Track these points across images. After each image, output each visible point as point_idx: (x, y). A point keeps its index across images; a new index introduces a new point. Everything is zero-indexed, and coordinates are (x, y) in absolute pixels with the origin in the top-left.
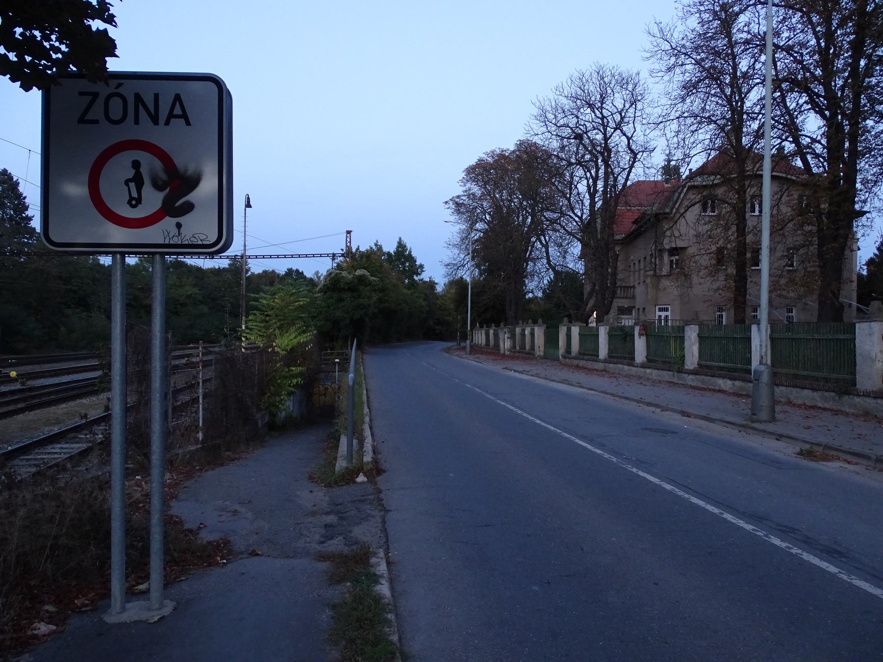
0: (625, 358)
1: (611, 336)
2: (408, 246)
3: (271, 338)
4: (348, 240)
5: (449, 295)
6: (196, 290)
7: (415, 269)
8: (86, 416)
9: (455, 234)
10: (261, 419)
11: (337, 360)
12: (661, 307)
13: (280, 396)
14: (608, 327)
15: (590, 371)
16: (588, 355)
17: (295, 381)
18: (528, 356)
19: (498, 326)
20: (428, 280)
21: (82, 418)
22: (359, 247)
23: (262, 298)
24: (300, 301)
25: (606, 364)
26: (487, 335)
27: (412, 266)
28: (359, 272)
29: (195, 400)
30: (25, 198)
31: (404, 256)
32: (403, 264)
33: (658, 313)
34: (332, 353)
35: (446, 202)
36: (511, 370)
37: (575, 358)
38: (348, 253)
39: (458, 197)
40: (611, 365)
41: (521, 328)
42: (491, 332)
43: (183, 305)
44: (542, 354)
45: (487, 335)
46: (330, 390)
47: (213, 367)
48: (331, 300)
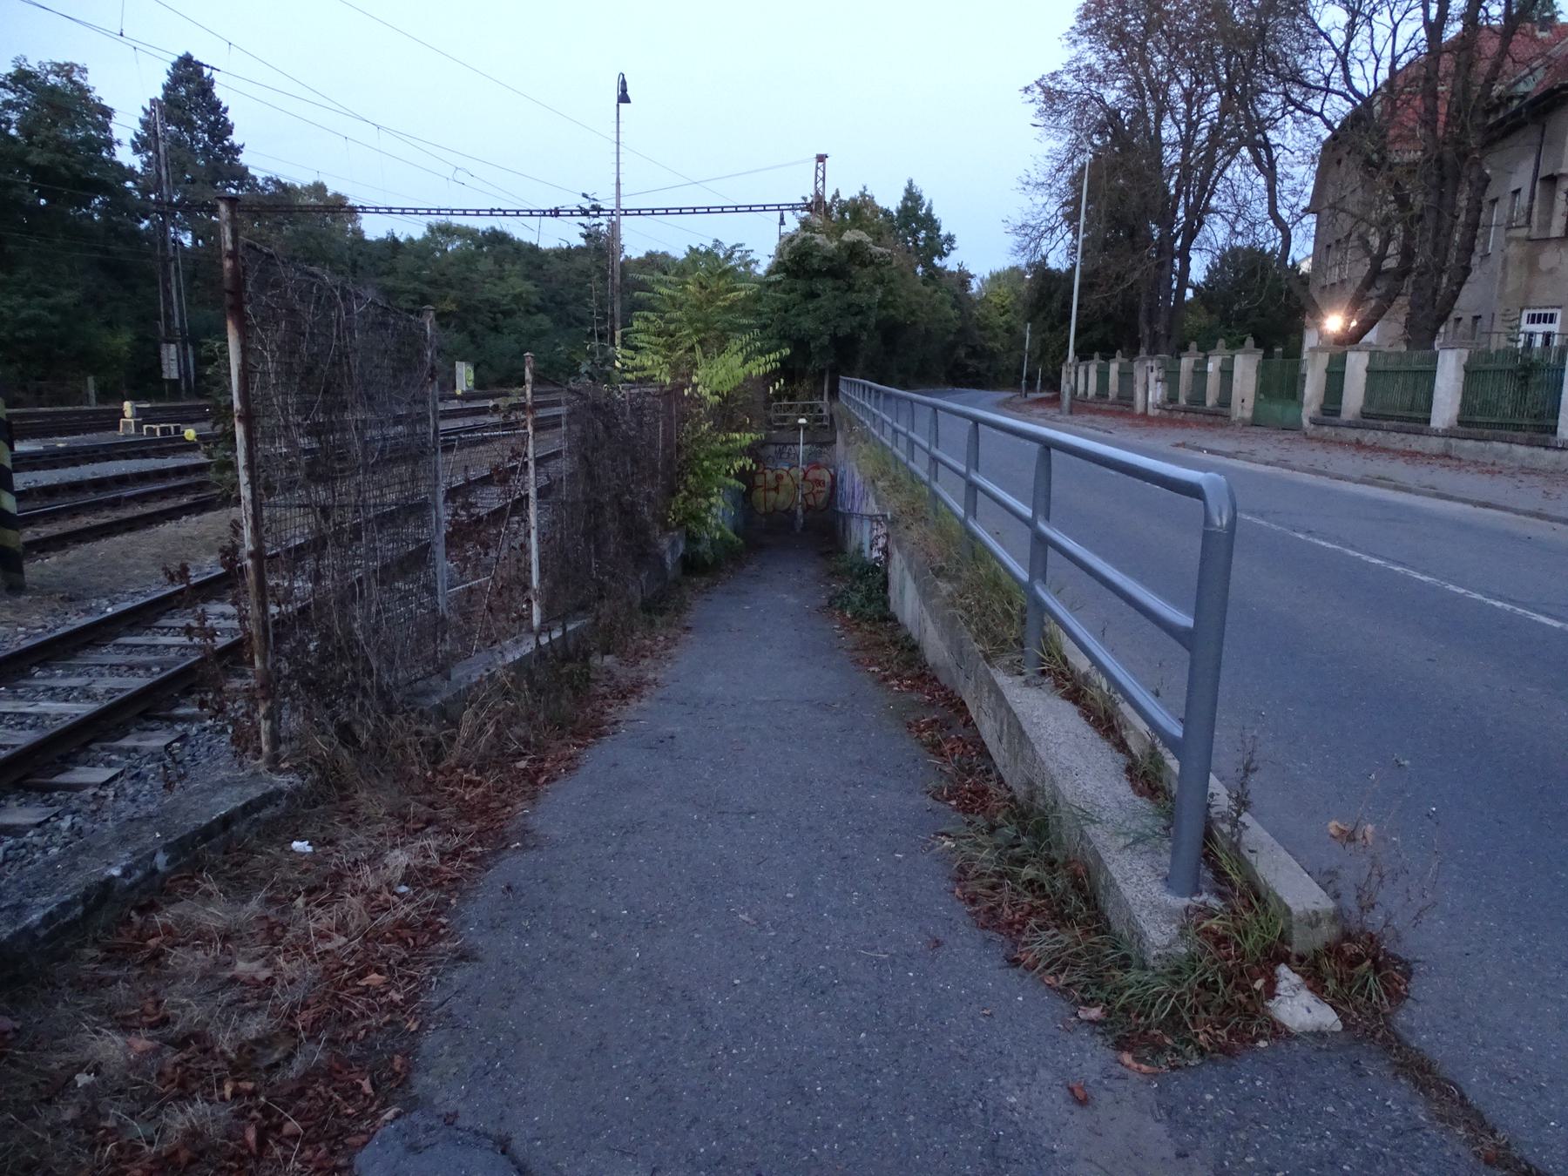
0: (1518, 428)
1: (1472, 373)
2: (926, 198)
3: (683, 371)
4: (820, 174)
5: (996, 300)
6: (528, 286)
7: (937, 244)
8: (184, 571)
9: (1043, 160)
10: (670, 548)
11: (802, 421)
12: (1537, 312)
13: (707, 496)
14: (1465, 353)
15: (1413, 455)
16: (1391, 418)
17: (738, 464)
18: (1210, 419)
19: (1132, 354)
20: (956, 269)
21: (172, 579)
22: (837, 192)
23: (659, 281)
24: (741, 289)
25: (1453, 442)
26: (1103, 375)
27: (932, 239)
28: (850, 236)
29: (520, 505)
30: (226, 110)
31: (918, 219)
32: (914, 233)
33: (1526, 327)
34: (791, 406)
35: (1027, 89)
36: (1200, 449)
37: (1351, 425)
38: (817, 205)
39: (1054, 76)
40: (1469, 444)
41: (1193, 359)
42: (1114, 368)
43: (508, 314)
44: (1248, 414)
45: (1103, 375)
46: (787, 480)
47: (564, 428)
48: (792, 295)
